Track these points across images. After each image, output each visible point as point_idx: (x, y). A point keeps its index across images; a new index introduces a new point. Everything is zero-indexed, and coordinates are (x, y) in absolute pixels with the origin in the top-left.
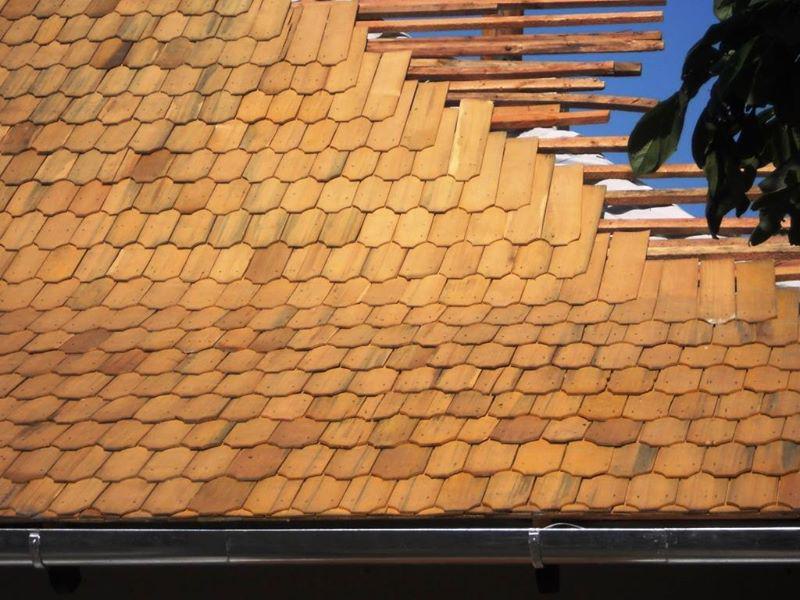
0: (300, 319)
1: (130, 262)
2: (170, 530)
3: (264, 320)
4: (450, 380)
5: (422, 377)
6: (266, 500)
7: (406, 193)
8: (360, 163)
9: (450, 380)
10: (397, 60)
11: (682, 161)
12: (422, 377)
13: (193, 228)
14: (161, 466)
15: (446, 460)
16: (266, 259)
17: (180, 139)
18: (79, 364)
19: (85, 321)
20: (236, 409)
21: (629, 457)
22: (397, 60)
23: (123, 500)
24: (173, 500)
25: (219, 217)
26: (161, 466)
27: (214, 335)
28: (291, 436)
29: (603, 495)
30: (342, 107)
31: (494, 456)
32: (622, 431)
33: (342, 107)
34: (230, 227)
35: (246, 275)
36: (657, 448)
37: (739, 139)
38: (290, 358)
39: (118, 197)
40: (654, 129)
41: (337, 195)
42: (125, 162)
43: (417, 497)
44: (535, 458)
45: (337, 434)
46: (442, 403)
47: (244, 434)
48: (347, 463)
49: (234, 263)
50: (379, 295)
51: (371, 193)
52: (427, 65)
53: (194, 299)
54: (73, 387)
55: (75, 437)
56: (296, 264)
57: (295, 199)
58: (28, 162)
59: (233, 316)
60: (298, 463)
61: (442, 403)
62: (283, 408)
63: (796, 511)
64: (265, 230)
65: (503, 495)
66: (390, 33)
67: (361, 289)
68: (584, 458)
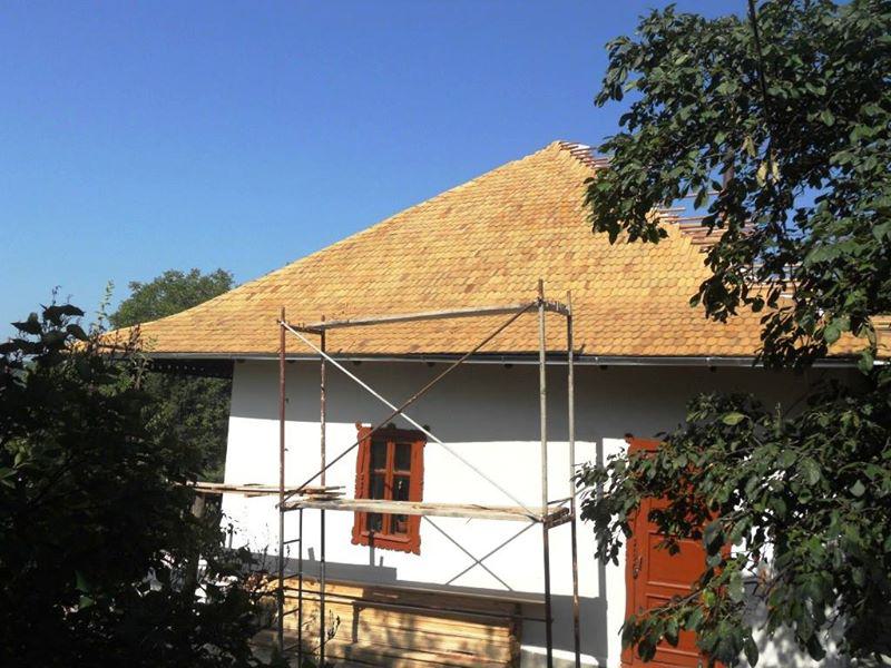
0: (661, 306)
1: (623, 291)
2: (626, 357)
3: (652, 306)
4: (695, 321)
5: (688, 321)
6: (648, 351)
7: (688, 274)
8: (678, 266)
9: (695, 321)
10: (689, 240)
11: (701, 304)
12: (688, 321)
13: (638, 282)
14: (626, 342)
15: (690, 342)
16: (654, 290)
17: (636, 261)
18: (609, 318)
19: (613, 306)
20: (644, 329)
21: (733, 341)
22: (689, 240)
23: (616, 351)
24: (627, 351)
25: (319, 337)
26: (626, 342)
27: (640, 310)
28: (656, 335)
29: (725, 351)
30: (674, 252)
31: (702, 341)
32: (733, 335)
33: (674, 252)
34: (646, 283)
35: (650, 294)
36: (740, 339)
37: (815, 369)
38: (657, 316)
39: (620, 276)
40: (135, 286)
41: (672, 274)
42: (620, 268)
43: (682, 351)
44: (711, 341)
45: (666, 335)
46: (692, 327)
47: (644, 335)
48: (667, 342)
49: (646, 292)
50: (681, 299)
51: (680, 273)
52: (695, 241)
53: (637, 301)
54: (607, 323)
55: (608, 335)
56: (661, 293)
57: (661, 276)
58: (600, 268)
59: (646, 305)
60: (656, 342)
61: (692, 327)
62: (654, 329)
63: (747, 3)
64: (653, 284)
65: (702, 350)
66: (687, 232)
67: (676, 298)
68: (723, 341)
